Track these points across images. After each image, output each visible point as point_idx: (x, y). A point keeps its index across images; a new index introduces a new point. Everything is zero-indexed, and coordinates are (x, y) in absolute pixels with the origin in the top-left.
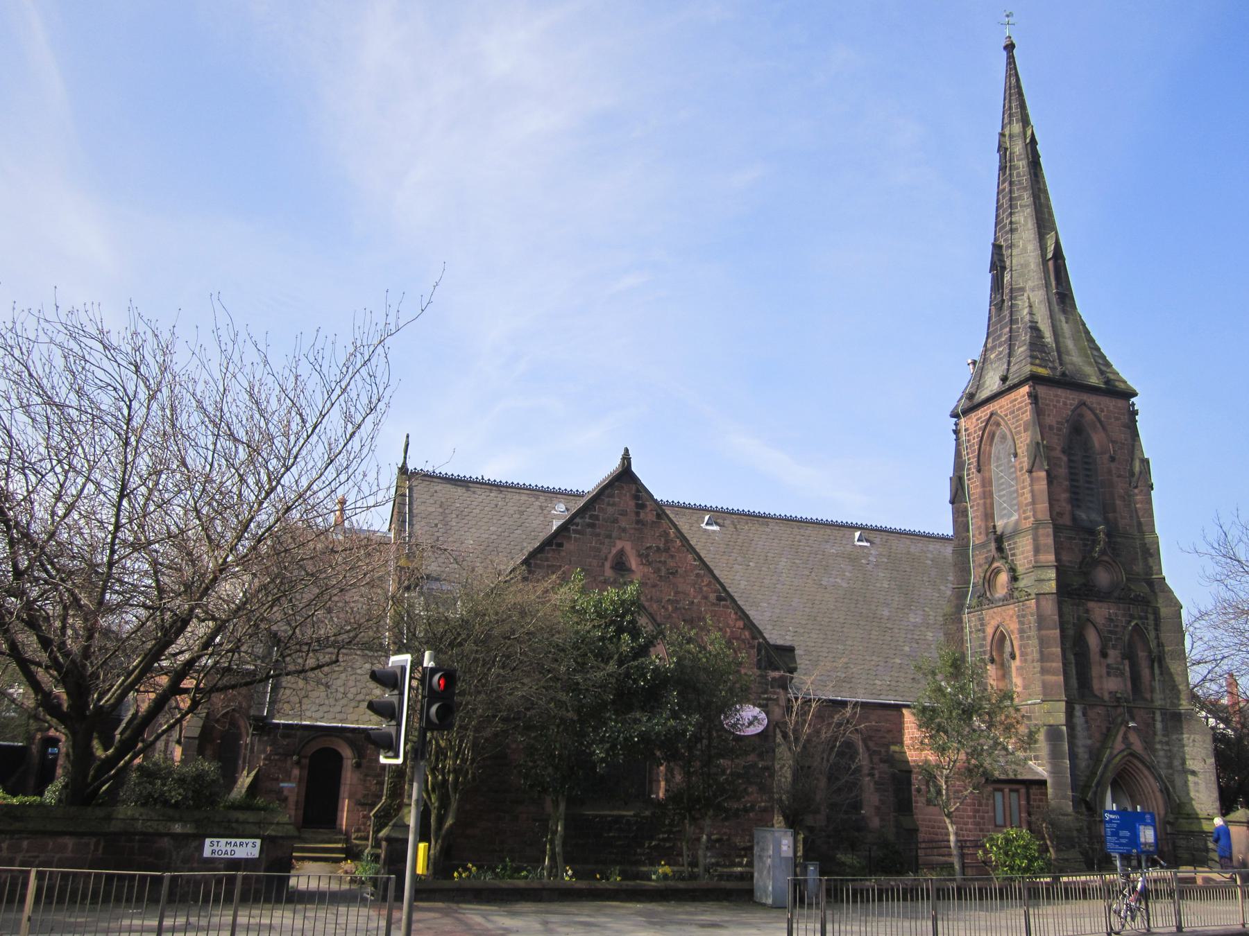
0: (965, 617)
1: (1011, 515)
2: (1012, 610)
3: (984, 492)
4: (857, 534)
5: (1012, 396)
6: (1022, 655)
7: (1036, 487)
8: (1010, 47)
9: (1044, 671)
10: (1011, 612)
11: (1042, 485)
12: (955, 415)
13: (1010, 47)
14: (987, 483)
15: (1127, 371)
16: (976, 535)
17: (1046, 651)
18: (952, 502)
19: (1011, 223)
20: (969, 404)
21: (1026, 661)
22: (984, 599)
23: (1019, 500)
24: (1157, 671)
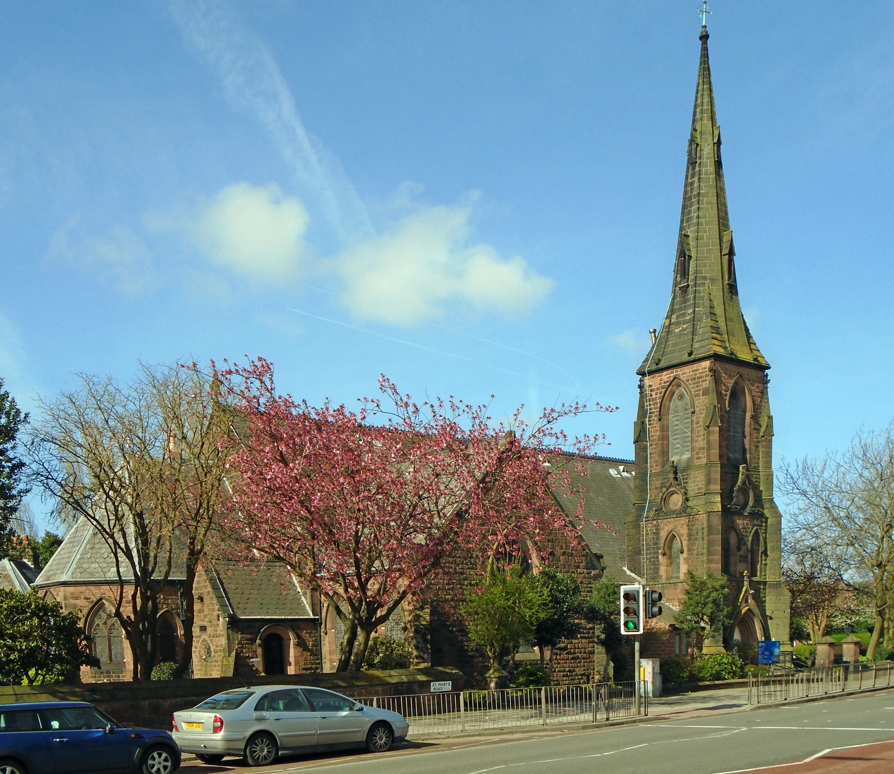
0: (643, 524)
1: (683, 453)
2: (683, 520)
3: (663, 435)
4: (621, 468)
5: (695, 366)
6: (689, 550)
7: (711, 438)
8: (704, 38)
9: (709, 561)
10: (683, 522)
11: (715, 437)
12: (642, 373)
13: (704, 38)
14: (664, 429)
15: (768, 351)
16: (653, 467)
17: (712, 549)
18: (636, 442)
19: (698, 217)
20: (654, 367)
21: (692, 554)
22: (661, 512)
23: (692, 443)
24: (151, 559)
